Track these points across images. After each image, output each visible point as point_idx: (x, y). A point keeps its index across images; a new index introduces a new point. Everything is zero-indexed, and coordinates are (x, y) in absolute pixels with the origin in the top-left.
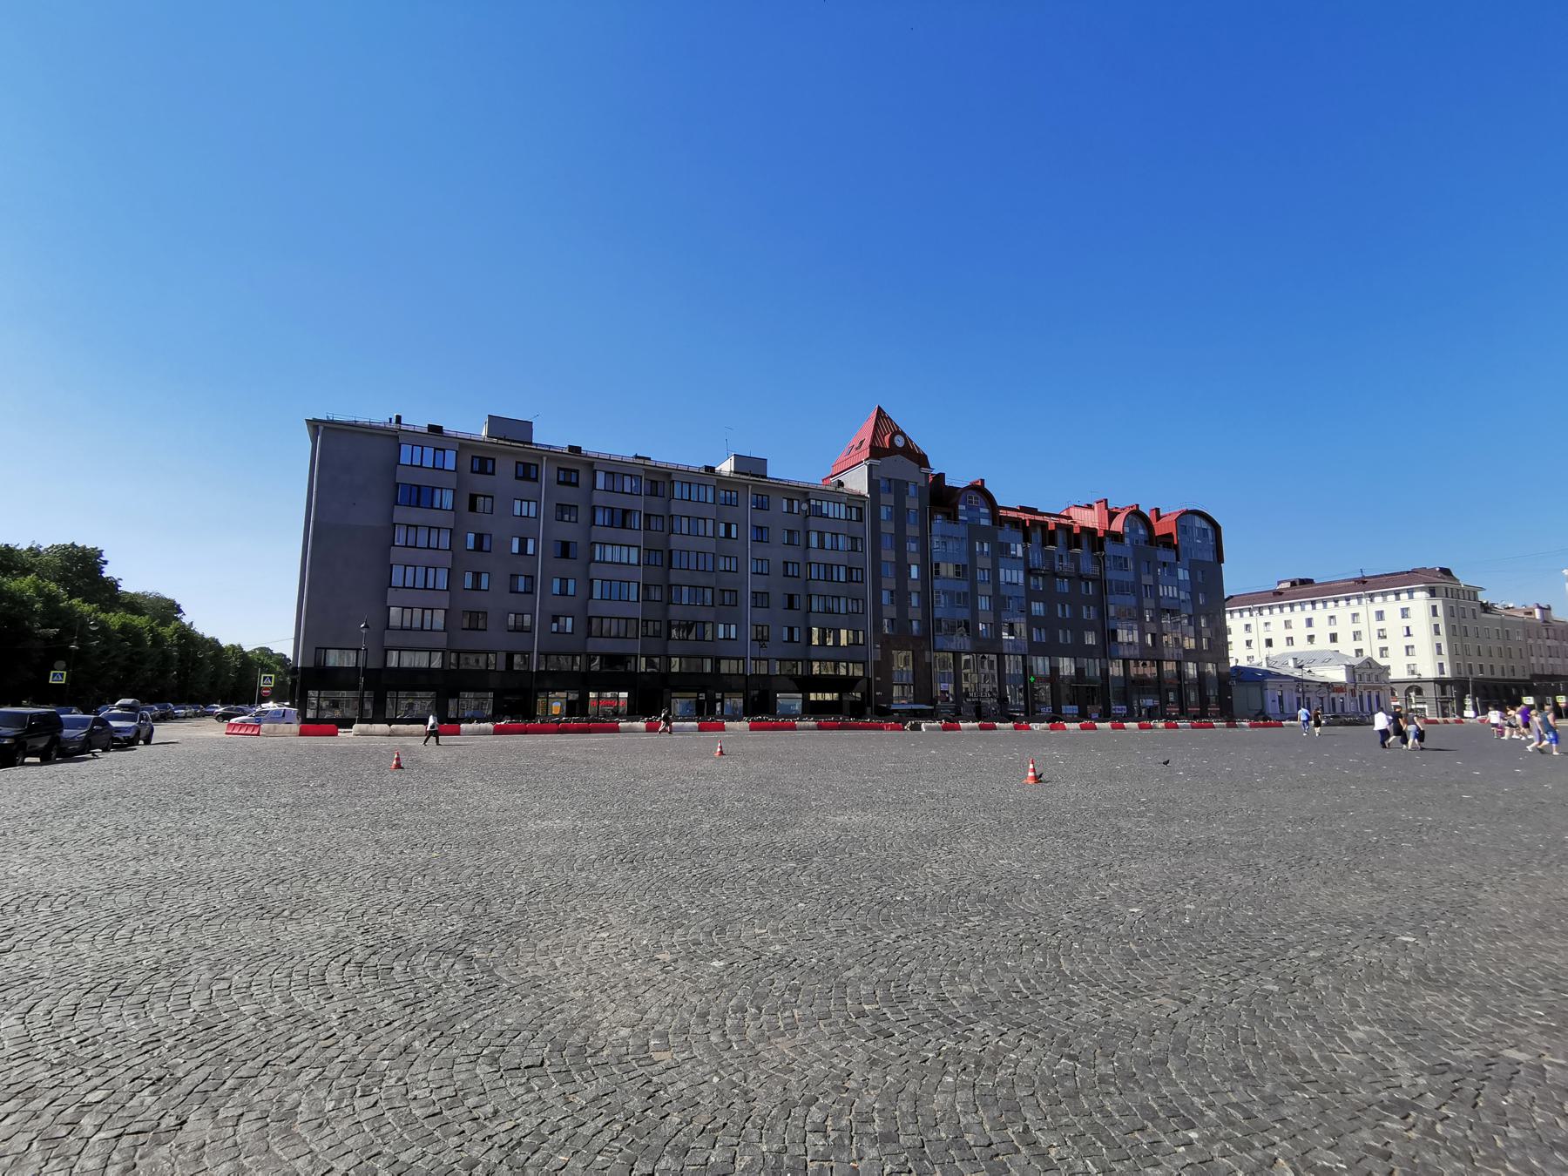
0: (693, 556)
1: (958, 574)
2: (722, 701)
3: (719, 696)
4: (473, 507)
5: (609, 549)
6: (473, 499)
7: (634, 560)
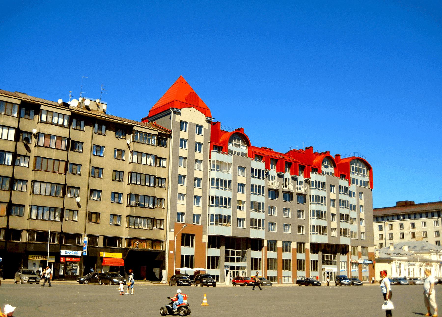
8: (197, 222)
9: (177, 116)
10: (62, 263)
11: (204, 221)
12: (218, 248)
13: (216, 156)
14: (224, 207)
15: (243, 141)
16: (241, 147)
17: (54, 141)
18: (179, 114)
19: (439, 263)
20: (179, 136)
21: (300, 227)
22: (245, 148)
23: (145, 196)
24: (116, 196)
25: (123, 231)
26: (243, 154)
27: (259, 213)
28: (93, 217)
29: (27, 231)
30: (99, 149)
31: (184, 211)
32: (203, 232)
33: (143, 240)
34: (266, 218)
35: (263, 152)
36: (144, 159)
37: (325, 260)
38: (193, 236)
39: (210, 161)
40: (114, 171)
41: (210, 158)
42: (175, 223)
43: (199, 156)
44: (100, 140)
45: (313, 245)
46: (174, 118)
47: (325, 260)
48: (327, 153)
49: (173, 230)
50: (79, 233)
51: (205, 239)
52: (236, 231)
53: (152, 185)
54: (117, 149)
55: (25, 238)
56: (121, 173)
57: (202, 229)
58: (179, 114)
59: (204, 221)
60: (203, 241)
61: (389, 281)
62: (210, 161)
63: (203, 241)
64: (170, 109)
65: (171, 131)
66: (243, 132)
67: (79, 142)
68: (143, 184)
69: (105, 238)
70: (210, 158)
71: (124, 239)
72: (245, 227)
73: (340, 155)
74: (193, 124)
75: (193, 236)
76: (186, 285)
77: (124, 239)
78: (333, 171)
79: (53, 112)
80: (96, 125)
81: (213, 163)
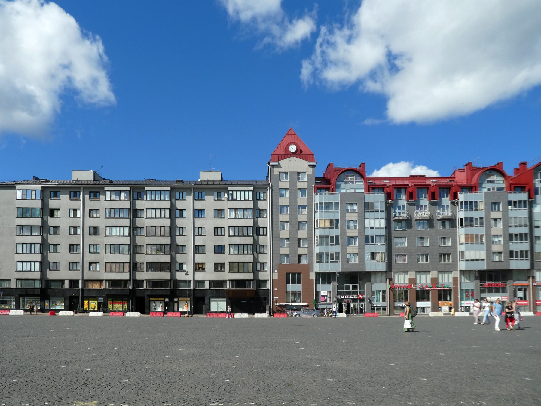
0: (29, 246)
1: (331, 225)
2: (178, 302)
3: (176, 300)
8: (427, 261)
10: (176, 302)
11: (310, 260)
12: (329, 282)
14: (331, 245)
15: (357, 175)
16: (357, 183)
18: (278, 166)
21: (444, 255)
22: (362, 183)
25: (227, 275)
26: (499, 189)
27: (472, 245)
29: (230, 281)
33: (101, 281)
34: (504, 250)
35: (406, 182)
37: (351, 290)
38: (299, 274)
43: (302, 201)
44: (199, 205)
45: (318, 274)
47: (351, 290)
48: (468, 164)
50: (265, 279)
51: (312, 276)
52: (345, 266)
55: (145, 286)
57: (308, 267)
58: (278, 166)
59: (310, 260)
60: (310, 278)
61: (169, 314)
63: (310, 278)
66: (502, 168)
67: (141, 210)
68: (241, 235)
71: (228, 282)
72: (429, 262)
73: (471, 163)
74: (293, 173)
75: (299, 274)
77: (228, 282)
78: (504, 185)
80: (216, 194)
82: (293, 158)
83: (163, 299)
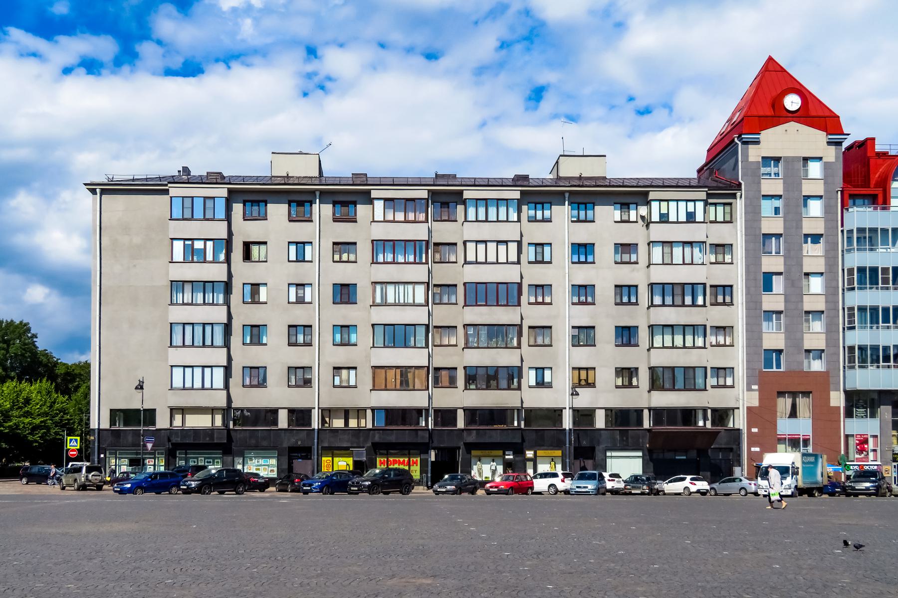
0: (199, 330)
3: (530, 454)
4: (247, 256)
5: (390, 289)
6: (247, 246)
7: (420, 299)
9: (752, 148)
10: (530, 460)
13: (861, 216)
17: (677, 251)
19: (886, 411)
20: (760, 191)
23: (684, 326)
24: (584, 335)
28: (301, 377)
30: (583, 251)
31: (781, 346)
32: (832, 386)
36: (677, 251)
39: (842, 231)
40: (616, 286)
41: (842, 225)
42: (761, 372)
46: (746, 155)
49: (755, 387)
53: (700, 301)
54: (621, 245)
56: (632, 289)
62: (842, 231)
64: (733, 140)
65: (740, 184)
69: (291, 411)
70: (842, 225)
76: (866, 493)
79: (507, 200)
81: (850, 235)
82: (793, 126)
83: (500, 453)
